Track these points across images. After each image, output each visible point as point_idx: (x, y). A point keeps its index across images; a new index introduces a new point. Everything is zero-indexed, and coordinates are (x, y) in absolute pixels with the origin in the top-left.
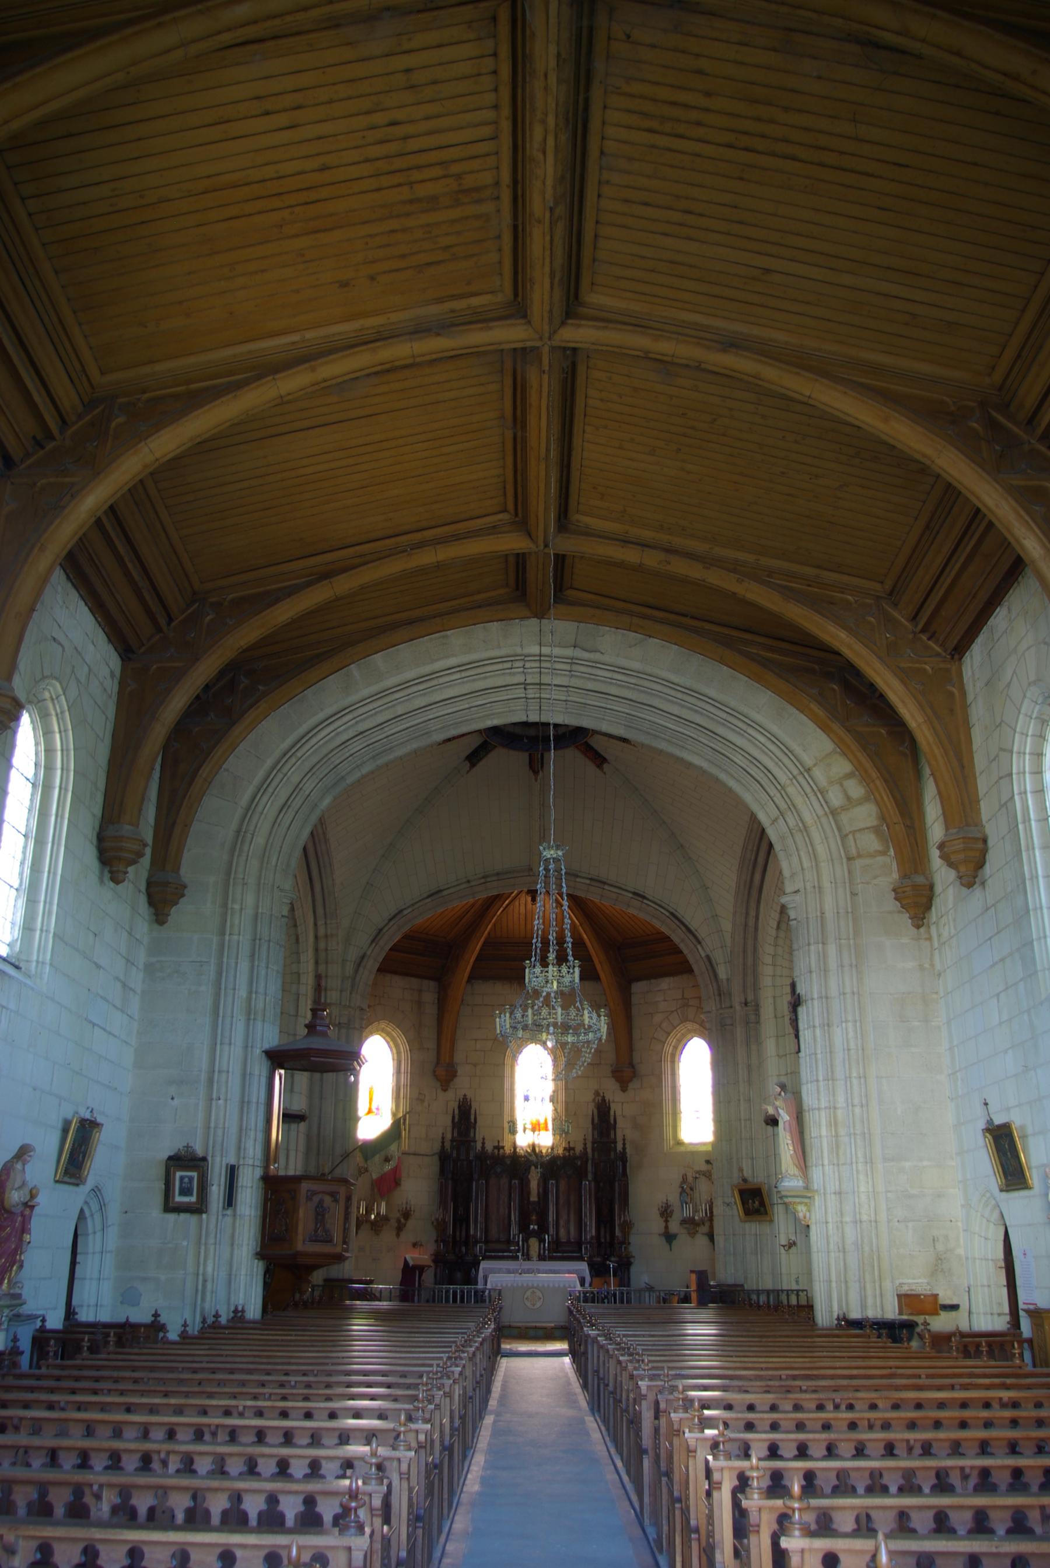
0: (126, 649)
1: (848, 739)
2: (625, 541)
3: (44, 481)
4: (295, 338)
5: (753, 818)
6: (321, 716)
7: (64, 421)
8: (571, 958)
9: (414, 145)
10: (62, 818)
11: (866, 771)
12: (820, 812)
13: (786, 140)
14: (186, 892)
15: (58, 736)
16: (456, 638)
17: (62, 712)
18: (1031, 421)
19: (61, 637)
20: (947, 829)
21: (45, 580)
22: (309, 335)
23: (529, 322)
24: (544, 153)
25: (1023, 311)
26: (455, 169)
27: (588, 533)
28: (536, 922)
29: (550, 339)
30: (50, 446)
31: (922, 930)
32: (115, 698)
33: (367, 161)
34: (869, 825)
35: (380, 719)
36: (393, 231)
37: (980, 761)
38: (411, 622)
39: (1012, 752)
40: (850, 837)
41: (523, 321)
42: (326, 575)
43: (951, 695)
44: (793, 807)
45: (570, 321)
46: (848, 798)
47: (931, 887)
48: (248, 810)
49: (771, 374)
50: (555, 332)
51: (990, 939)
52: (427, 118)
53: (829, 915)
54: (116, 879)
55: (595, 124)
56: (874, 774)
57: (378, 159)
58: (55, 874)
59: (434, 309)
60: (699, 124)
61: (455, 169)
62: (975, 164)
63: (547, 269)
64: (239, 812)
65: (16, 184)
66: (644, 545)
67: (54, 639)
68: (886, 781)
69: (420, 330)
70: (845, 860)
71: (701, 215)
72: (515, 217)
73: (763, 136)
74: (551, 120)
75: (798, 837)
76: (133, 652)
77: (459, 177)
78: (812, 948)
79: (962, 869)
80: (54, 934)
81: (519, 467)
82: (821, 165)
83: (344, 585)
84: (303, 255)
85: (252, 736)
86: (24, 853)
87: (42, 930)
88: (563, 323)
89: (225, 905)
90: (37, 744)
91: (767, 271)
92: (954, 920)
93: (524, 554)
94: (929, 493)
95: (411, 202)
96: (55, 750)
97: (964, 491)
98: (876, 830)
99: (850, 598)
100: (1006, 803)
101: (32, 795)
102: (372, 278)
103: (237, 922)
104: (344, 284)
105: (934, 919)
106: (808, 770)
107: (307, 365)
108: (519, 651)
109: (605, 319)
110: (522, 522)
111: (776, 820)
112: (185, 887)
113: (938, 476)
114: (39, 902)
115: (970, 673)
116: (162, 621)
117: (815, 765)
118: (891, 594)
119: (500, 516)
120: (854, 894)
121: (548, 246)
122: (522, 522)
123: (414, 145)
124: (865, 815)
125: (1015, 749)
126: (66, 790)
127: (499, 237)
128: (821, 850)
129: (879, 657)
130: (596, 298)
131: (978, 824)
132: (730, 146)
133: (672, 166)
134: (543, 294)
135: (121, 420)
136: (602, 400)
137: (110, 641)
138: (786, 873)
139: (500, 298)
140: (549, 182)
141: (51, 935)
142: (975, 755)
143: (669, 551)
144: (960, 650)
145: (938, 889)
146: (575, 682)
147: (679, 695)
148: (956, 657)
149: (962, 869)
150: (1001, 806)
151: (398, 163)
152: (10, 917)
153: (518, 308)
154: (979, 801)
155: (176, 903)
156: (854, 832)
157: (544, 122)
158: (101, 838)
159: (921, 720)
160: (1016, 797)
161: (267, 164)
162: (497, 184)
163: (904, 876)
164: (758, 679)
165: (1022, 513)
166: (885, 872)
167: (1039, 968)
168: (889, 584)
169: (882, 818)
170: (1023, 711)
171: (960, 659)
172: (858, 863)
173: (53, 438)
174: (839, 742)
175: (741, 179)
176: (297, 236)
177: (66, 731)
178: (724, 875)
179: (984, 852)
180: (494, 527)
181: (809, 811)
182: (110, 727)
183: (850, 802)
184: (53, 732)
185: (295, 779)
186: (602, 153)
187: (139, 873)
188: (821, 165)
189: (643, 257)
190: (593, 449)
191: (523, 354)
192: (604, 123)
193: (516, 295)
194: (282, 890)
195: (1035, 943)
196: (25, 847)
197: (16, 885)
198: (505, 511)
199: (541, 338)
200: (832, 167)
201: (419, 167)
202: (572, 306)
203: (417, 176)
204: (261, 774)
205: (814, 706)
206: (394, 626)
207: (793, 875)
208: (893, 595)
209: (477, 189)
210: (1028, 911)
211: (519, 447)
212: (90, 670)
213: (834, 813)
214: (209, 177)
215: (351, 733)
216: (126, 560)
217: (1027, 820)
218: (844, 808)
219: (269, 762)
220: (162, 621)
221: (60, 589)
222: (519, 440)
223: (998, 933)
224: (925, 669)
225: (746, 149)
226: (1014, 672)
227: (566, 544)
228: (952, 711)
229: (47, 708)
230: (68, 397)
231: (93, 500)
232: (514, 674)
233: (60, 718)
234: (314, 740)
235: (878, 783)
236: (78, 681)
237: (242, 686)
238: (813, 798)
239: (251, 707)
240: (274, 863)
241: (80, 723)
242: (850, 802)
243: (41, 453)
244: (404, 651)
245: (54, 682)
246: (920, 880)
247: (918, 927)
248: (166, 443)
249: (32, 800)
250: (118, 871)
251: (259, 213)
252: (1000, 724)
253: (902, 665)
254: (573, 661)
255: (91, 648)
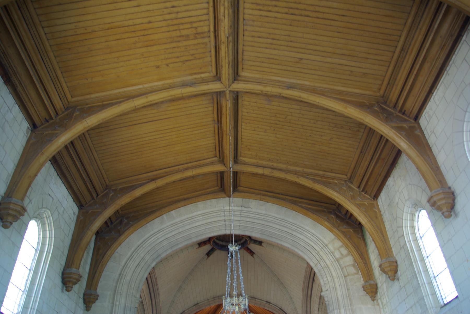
0: (80, 206)
1: (339, 233)
2: (258, 166)
3: (47, 133)
4: (141, 86)
5: (308, 263)
6: (152, 232)
7: (57, 114)
8: (244, 294)
9: (181, 15)
10: (46, 263)
11: (347, 245)
12: (333, 260)
13: (305, 10)
14: (99, 298)
15: (48, 232)
16: (200, 205)
17: (51, 223)
18: (395, 106)
19: (52, 194)
20: (381, 259)
21: (42, 165)
22: (146, 86)
23: (222, 82)
24: (224, 17)
25: (389, 67)
26: (195, 25)
27: (244, 164)
28: (227, 279)
29: (229, 87)
30: (51, 121)
31: (375, 302)
32: (75, 222)
33: (165, 20)
34: (350, 263)
35: (173, 233)
36: (174, 47)
37: (390, 234)
38: (184, 199)
39: (403, 227)
40: (344, 268)
41: (219, 82)
42: (154, 179)
43: (375, 212)
44: (322, 259)
45: (235, 82)
46: (342, 255)
47: (376, 285)
48: (124, 267)
49: (305, 96)
50: (230, 85)
51: (404, 300)
52: (185, 5)
53: (340, 298)
54: (68, 290)
55: (241, 9)
56: (350, 245)
57: (168, 20)
58: (40, 285)
59: (189, 78)
60: (276, 6)
61: (195, 25)
62: (369, 13)
63: (227, 61)
64: (121, 267)
65: (40, 22)
66: (264, 167)
67: (49, 195)
68: (355, 247)
69: (184, 85)
70: (343, 277)
71: (278, 40)
72: (216, 43)
73: (297, 9)
74: (226, 4)
75: (326, 270)
76: (83, 206)
77: (196, 28)
78: (335, 311)
79: (390, 273)
80: (37, 310)
81: (220, 139)
82: (318, 18)
83: (160, 183)
84: (143, 55)
85: (127, 240)
86: (28, 277)
87: (31, 308)
88: (233, 82)
89: (113, 303)
90: (39, 235)
91: (301, 59)
92: (388, 296)
93: (223, 172)
94: (361, 139)
95: (180, 36)
96: (47, 238)
97: (376, 129)
98: (353, 266)
99: (336, 181)
100: (403, 246)
101: (35, 254)
102: (167, 65)
103: (117, 309)
104: (158, 67)
105: (379, 297)
106: (327, 245)
107: (145, 96)
108: (222, 208)
109: (247, 81)
110: (222, 161)
111: (317, 264)
112: (98, 296)
113: (366, 126)
114: (32, 297)
115: (381, 204)
116: (95, 195)
117: (329, 243)
118: (350, 179)
119: (214, 159)
120: (348, 290)
121: (227, 51)
122: (222, 161)
123: (181, 15)
124: (349, 260)
125: (404, 225)
126: (49, 253)
127: (210, 51)
128: (334, 274)
129: (349, 200)
130: (243, 74)
131: (393, 256)
132: (287, 13)
133: (267, 22)
134: (226, 71)
135: (77, 113)
136: (247, 113)
137: (74, 201)
138: (322, 283)
139: (211, 74)
140: (227, 27)
141: (35, 310)
142: (388, 233)
143: (272, 168)
144: (376, 196)
145: (379, 285)
146: (242, 219)
147: (279, 221)
148: (375, 199)
149: (390, 273)
150: (401, 248)
151: (175, 22)
152: (18, 303)
153: (218, 77)
154: (391, 248)
155: (95, 302)
156: (345, 267)
157: (224, 5)
158: (63, 274)
159: (366, 221)
160: (407, 243)
161: (130, 20)
162: (209, 31)
163: (366, 281)
164: (306, 215)
165: (398, 134)
166: (358, 281)
167: (428, 307)
168: (349, 175)
169: (355, 261)
170: (405, 211)
171: (377, 200)
172: (348, 278)
173: (52, 119)
174: (336, 235)
175: (291, 25)
176: (141, 48)
177: (51, 230)
178: (297, 292)
179: (397, 267)
180: (212, 163)
181: (329, 260)
182: (71, 232)
183: (343, 256)
184: (46, 231)
185: (142, 255)
186: (244, 19)
187: (79, 288)
188: (318, 18)
189: (259, 57)
190: (245, 131)
191: (220, 94)
192: (244, 8)
193: (217, 74)
194: (135, 297)
195: (425, 298)
196: (29, 274)
197: (23, 289)
198: (216, 157)
199: (226, 88)
200: (321, 18)
201: (182, 24)
202: (236, 77)
203: (182, 27)
204: (129, 254)
205: (326, 223)
206: (179, 201)
207: (325, 284)
208: (351, 180)
209: (202, 33)
210: (419, 286)
211: (220, 131)
212: (64, 209)
213: (338, 260)
214: (109, 23)
215: (163, 238)
216: (80, 169)
217: (412, 251)
218: (340, 258)
219: (133, 249)
220: (95, 195)
221: (53, 177)
222: (220, 129)
223: (408, 297)
224: (365, 204)
225: (292, 14)
226: (399, 198)
227: (238, 168)
228: (377, 217)
229: (44, 221)
230: (59, 104)
231: (64, 138)
232: (221, 216)
233: (50, 225)
234: (150, 241)
235: (352, 248)
236: (59, 212)
237: (124, 222)
238: (329, 255)
239: (127, 229)
240: (133, 286)
241: (58, 228)
242: (343, 256)
243: (47, 124)
244: (182, 209)
245: (47, 210)
246: (372, 282)
247: (373, 300)
248: (92, 121)
249: (34, 256)
250: (69, 287)
251: (128, 38)
252: (396, 218)
253: (357, 203)
254: (241, 211)
255: (66, 202)
